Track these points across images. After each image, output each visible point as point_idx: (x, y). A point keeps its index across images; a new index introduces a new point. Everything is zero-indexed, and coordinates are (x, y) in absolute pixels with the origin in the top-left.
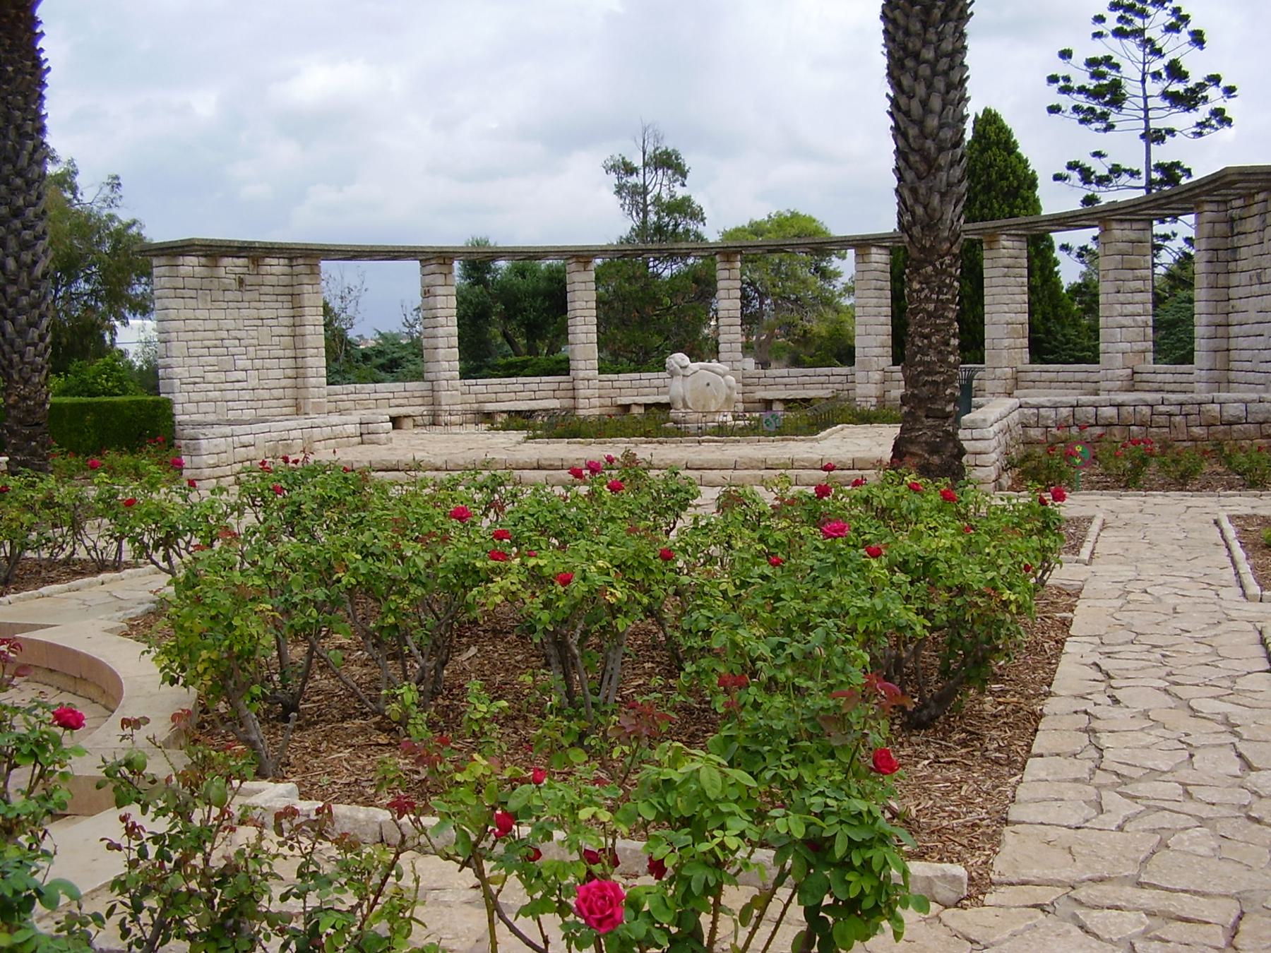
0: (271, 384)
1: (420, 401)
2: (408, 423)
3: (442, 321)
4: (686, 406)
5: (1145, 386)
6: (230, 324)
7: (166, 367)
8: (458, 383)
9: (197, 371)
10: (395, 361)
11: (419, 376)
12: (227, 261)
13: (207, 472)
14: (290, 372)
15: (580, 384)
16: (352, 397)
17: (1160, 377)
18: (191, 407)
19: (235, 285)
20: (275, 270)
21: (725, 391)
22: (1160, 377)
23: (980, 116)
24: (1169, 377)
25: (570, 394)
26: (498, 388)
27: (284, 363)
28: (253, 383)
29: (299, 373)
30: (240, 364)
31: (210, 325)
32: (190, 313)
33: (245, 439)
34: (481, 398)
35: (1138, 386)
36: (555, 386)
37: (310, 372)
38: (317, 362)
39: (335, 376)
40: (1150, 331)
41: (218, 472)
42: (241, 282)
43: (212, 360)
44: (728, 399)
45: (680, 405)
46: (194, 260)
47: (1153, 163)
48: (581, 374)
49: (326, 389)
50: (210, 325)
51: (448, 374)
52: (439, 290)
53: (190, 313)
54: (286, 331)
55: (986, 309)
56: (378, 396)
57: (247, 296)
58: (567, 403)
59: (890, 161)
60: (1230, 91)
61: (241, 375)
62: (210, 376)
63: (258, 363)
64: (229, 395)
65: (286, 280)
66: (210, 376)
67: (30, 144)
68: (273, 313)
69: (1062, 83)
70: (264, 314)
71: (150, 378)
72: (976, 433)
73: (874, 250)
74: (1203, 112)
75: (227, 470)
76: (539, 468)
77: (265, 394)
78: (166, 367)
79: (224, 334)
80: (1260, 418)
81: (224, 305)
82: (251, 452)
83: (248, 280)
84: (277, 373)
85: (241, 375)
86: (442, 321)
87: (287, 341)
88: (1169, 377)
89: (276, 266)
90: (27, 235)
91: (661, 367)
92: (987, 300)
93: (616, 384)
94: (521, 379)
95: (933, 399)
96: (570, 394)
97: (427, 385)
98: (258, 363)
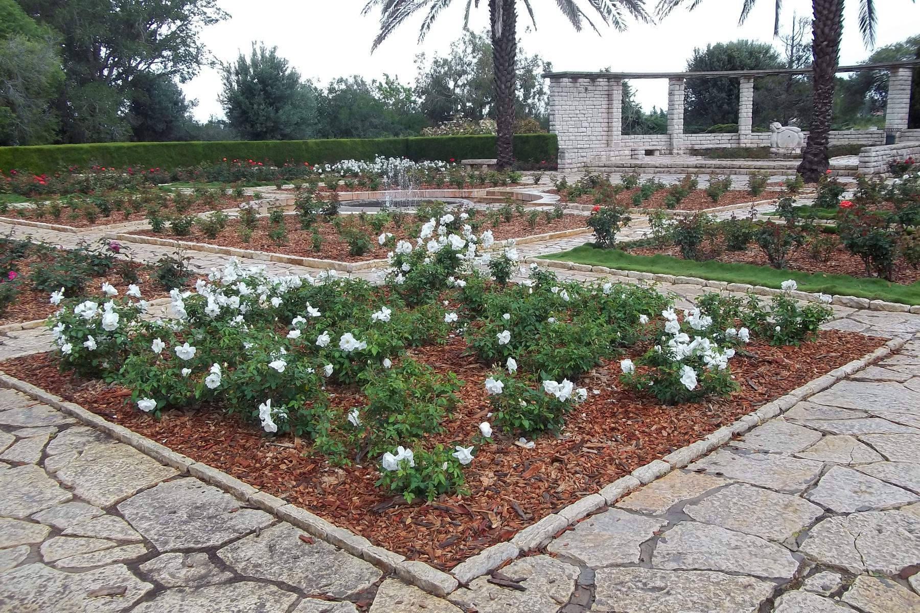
0: (596, 134)
2: (657, 153)
3: (677, 107)
4: (778, 146)
9: (565, 128)
10: (657, 125)
12: (581, 80)
13: (567, 166)
14: (606, 129)
15: (742, 137)
19: (583, 91)
20: (601, 84)
21: (797, 140)
28: (589, 133)
29: (609, 129)
32: (564, 103)
33: (583, 154)
34: (693, 142)
38: (617, 125)
39: (625, 132)
41: (571, 166)
42: (586, 89)
44: (799, 144)
45: (775, 146)
48: (743, 132)
49: (621, 137)
50: (573, 108)
52: (676, 92)
53: (564, 103)
54: (604, 111)
62: (571, 130)
64: (579, 138)
65: (606, 88)
68: (599, 103)
70: (595, 103)
71: (546, 123)
72: (866, 154)
73: (901, 70)
75: (575, 166)
77: (594, 138)
83: (590, 88)
84: (600, 129)
86: (677, 107)
89: (602, 82)
91: (768, 129)
95: (817, 138)
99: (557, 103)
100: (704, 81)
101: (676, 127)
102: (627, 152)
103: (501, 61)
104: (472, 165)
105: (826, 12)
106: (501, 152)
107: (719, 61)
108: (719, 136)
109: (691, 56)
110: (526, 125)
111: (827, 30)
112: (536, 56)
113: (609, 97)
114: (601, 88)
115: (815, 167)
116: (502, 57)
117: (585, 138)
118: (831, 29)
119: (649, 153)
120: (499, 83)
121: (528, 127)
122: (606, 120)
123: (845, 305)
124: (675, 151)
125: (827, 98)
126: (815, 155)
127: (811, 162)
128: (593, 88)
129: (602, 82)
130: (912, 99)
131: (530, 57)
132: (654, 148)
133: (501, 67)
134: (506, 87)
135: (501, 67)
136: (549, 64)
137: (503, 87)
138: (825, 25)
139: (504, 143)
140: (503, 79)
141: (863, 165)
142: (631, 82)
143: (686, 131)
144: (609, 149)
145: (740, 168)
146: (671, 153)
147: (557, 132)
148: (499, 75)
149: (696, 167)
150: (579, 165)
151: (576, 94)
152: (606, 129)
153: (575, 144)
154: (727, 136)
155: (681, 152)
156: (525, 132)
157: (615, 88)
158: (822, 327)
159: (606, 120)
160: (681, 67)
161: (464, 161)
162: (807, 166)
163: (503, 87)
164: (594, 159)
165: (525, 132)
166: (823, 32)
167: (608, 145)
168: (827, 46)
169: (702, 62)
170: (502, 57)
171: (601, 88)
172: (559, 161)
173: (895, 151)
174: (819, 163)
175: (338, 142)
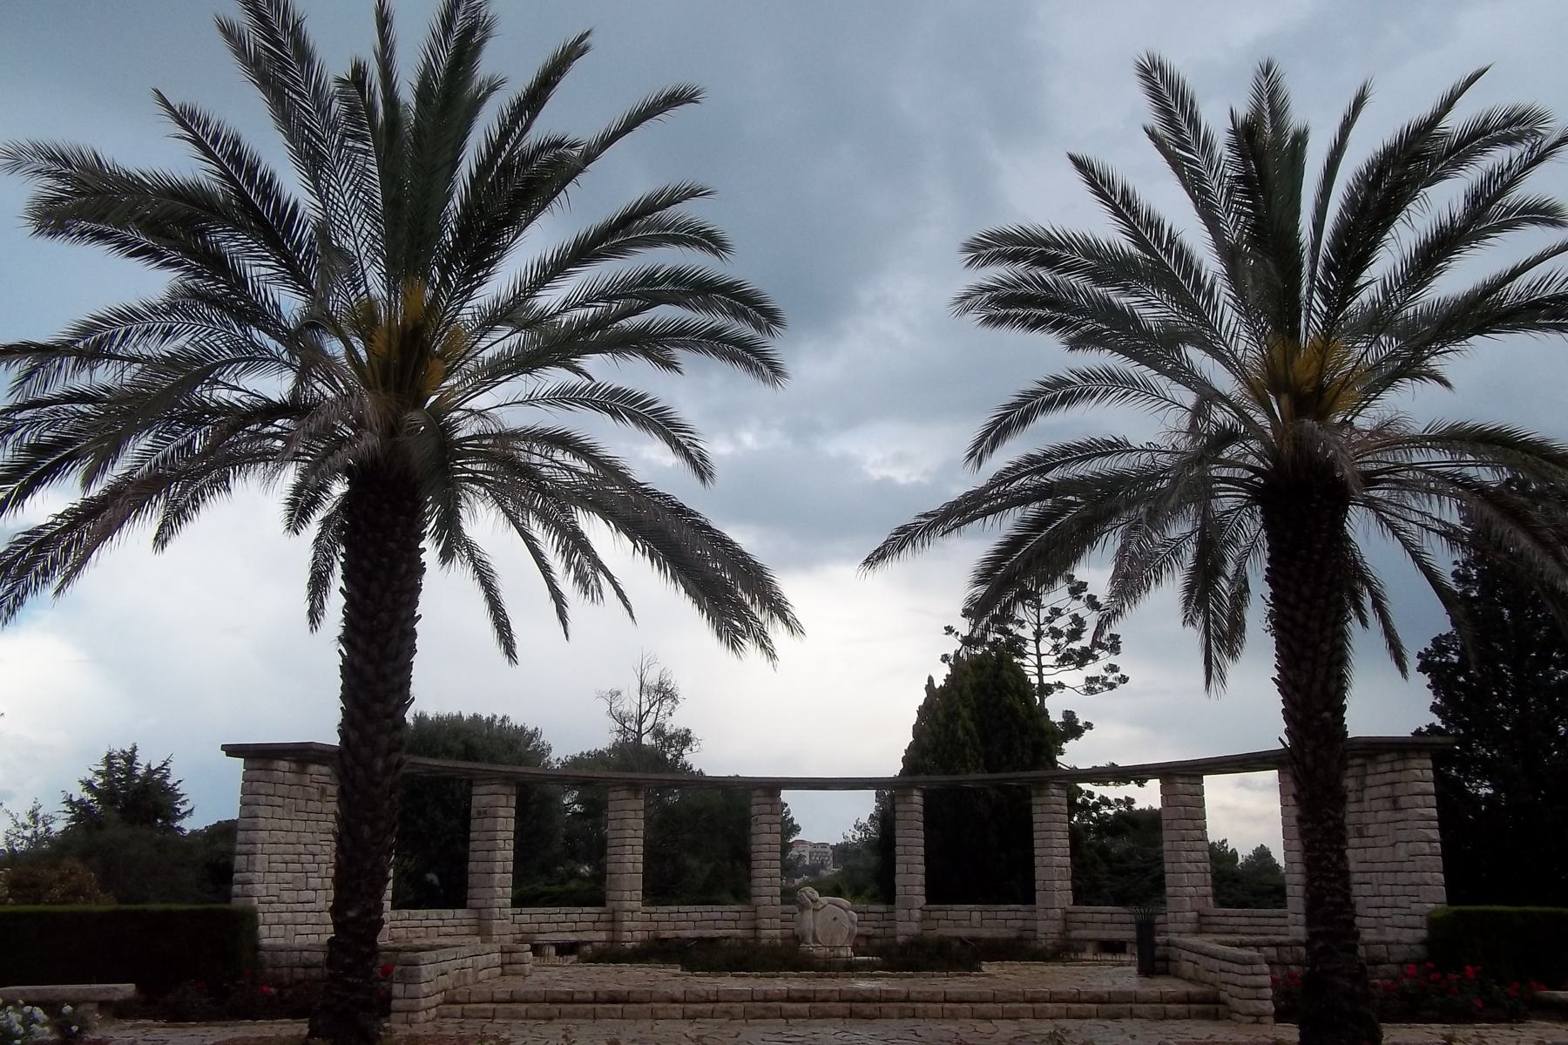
1: (466, 930)
4: (815, 940)
5: (1216, 928)
6: (308, 837)
7: (243, 883)
8: (510, 911)
9: (274, 889)
11: (599, 901)
12: (313, 768)
16: (406, 923)
17: (1232, 920)
18: (278, 930)
22: (1232, 920)
24: (1244, 921)
25: (752, 924)
26: (541, 918)
31: (292, 837)
35: (1205, 928)
36: (595, 917)
40: (1209, 876)
43: (288, 876)
50: (292, 837)
51: (500, 902)
55: (1036, 852)
56: (429, 923)
58: (750, 933)
59: (338, 717)
61: (311, 895)
64: (300, 917)
66: (286, 895)
74: (1093, 669)
76: (572, 1002)
78: (243, 883)
79: (301, 848)
80: (1400, 958)
81: (305, 816)
85: (311, 895)
88: (1244, 921)
92: (1037, 843)
93: (655, 917)
94: (564, 910)
96: (609, 926)
97: (473, 914)
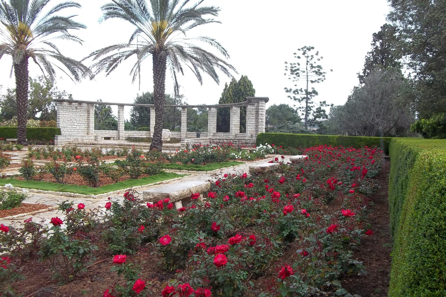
13: (59, 143)
14: (86, 127)
19: (75, 108)
21: (168, 135)
23: (228, 84)
27: (85, 125)
28: (78, 128)
29: (88, 127)
30: (75, 124)
31: (69, 116)
32: (64, 114)
33: (68, 138)
37: (90, 127)
38: (92, 125)
41: (61, 143)
42: (76, 108)
44: (169, 136)
46: (66, 103)
47: (111, 106)
49: (94, 131)
50: (70, 116)
53: (64, 114)
54: (86, 118)
57: (78, 111)
60: (325, 79)
62: (68, 126)
63: (79, 124)
64: (72, 130)
65: (87, 108)
67: (25, 84)
69: (316, 69)
70: (81, 114)
75: (64, 143)
77: (81, 131)
82: (69, 140)
83: (78, 107)
84: (84, 127)
87: (86, 120)
90: (24, 99)
98: (79, 124)
99: (60, 113)
100: (141, 108)
101: (121, 127)
102: (93, 138)
103: (20, 91)
104: (12, 142)
105: (158, 83)
106: (20, 135)
107: (147, 99)
108: (141, 132)
109: (135, 97)
110: (50, 123)
111: (158, 90)
112: (64, 91)
113: (88, 112)
114: (84, 108)
115: (156, 146)
116: (20, 90)
117: (74, 130)
118: (160, 90)
119: (107, 138)
120: (18, 102)
121: (51, 124)
122: (87, 123)
123: (66, 196)
124: (121, 138)
125: (160, 117)
126: (156, 141)
127: (154, 144)
128: (80, 108)
129: (85, 105)
130: (217, 120)
131: (62, 91)
132: (111, 136)
133: (20, 95)
134: (22, 104)
135: (20, 95)
136: (71, 95)
137: (21, 104)
138: (158, 88)
139: (21, 131)
140: (21, 100)
141: (182, 146)
142: (111, 106)
143: (95, 129)
144: (88, 136)
145: (137, 146)
146: (119, 139)
147: (61, 127)
148: (19, 98)
149: (119, 145)
150: (66, 143)
151: (71, 110)
152: (86, 127)
153: (70, 133)
154: (145, 132)
155: (124, 139)
156: (49, 127)
157: (91, 108)
158: (24, 202)
159: (87, 123)
160: (132, 102)
161: (8, 140)
162: (153, 145)
163: (21, 104)
164: (74, 140)
165: (49, 127)
166: (157, 90)
167: (88, 134)
168: (159, 96)
169: (140, 100)
170: (20, 90)
171: (84, 108)
172: (55, 141)
173: (218, 140)
174: (158, 144)
175: (294, 135)
